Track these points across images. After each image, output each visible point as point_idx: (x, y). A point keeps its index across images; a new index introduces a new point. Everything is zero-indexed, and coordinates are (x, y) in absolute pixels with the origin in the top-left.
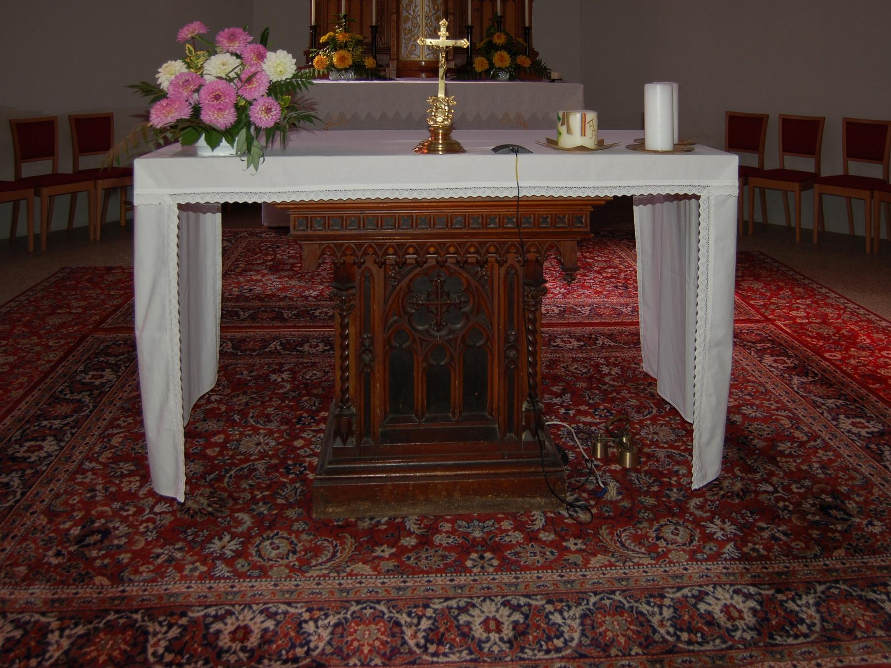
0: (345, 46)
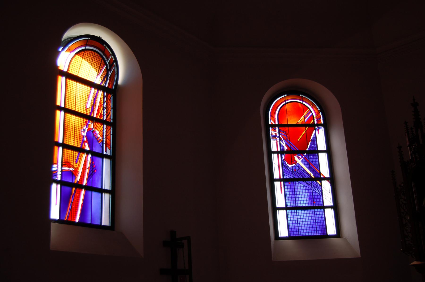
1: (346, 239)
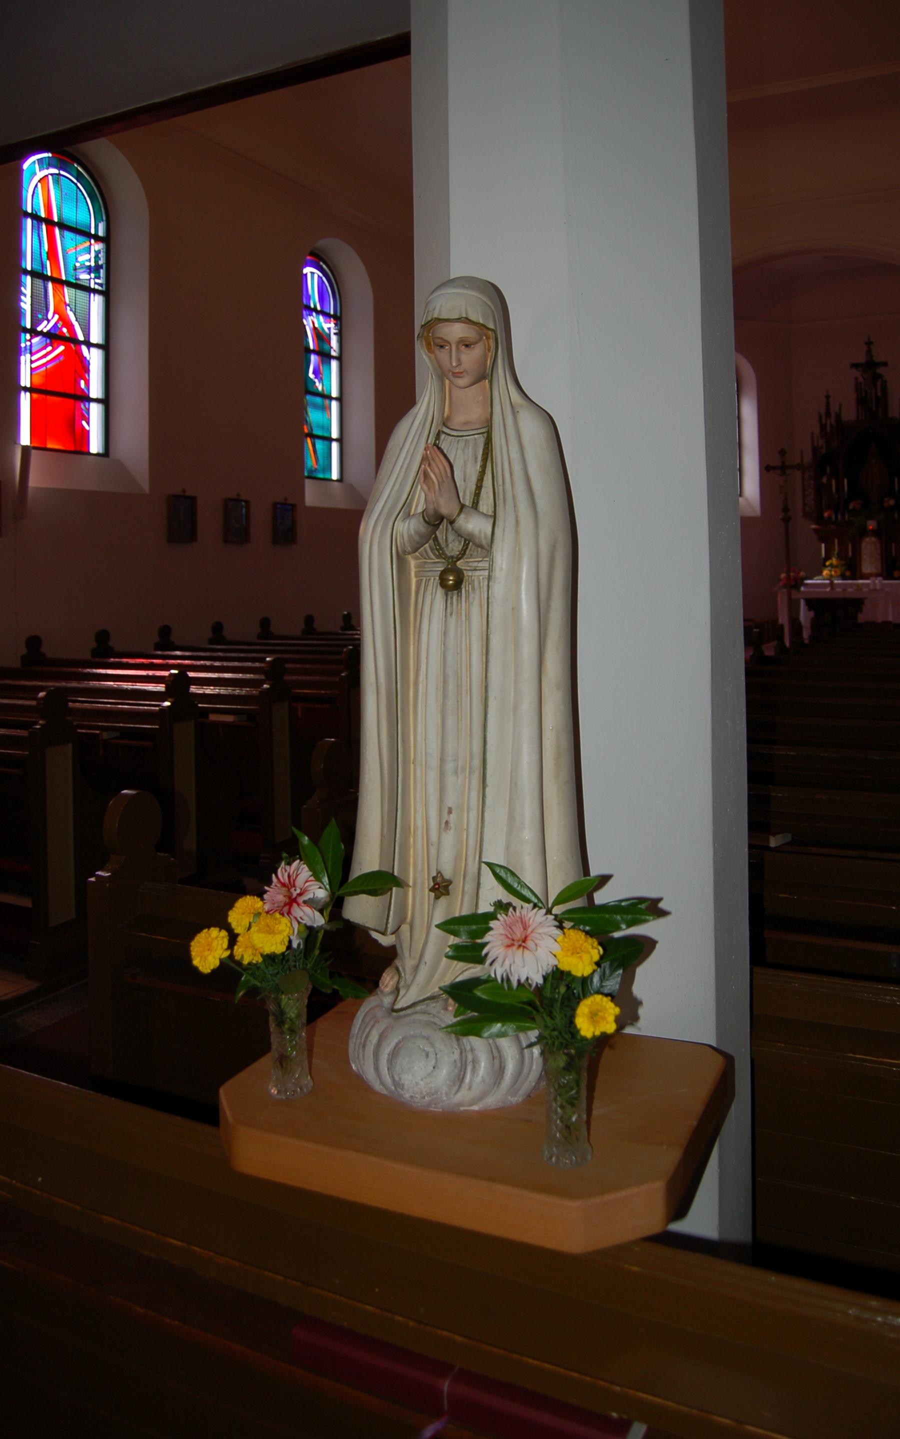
0: (836, 567)
1: (747, 499)
